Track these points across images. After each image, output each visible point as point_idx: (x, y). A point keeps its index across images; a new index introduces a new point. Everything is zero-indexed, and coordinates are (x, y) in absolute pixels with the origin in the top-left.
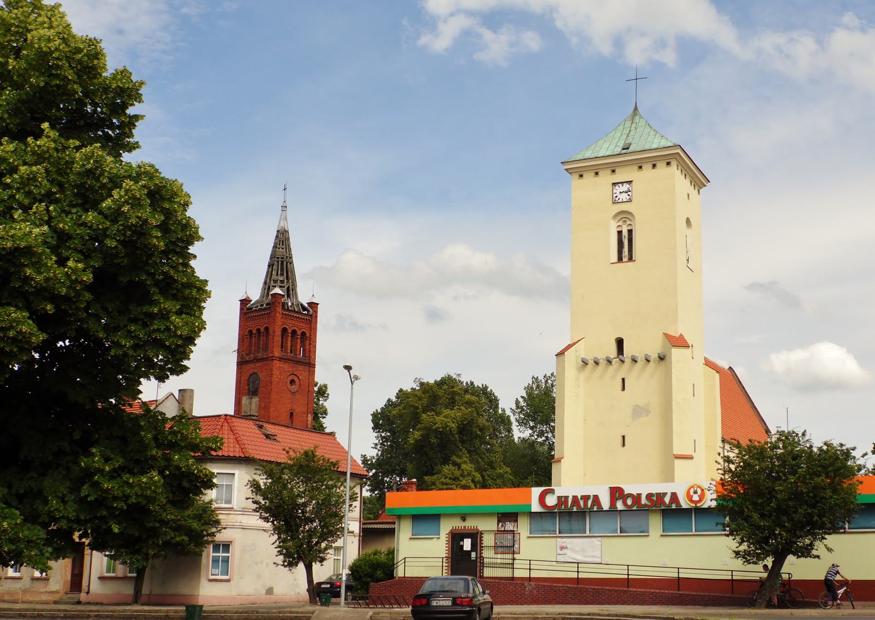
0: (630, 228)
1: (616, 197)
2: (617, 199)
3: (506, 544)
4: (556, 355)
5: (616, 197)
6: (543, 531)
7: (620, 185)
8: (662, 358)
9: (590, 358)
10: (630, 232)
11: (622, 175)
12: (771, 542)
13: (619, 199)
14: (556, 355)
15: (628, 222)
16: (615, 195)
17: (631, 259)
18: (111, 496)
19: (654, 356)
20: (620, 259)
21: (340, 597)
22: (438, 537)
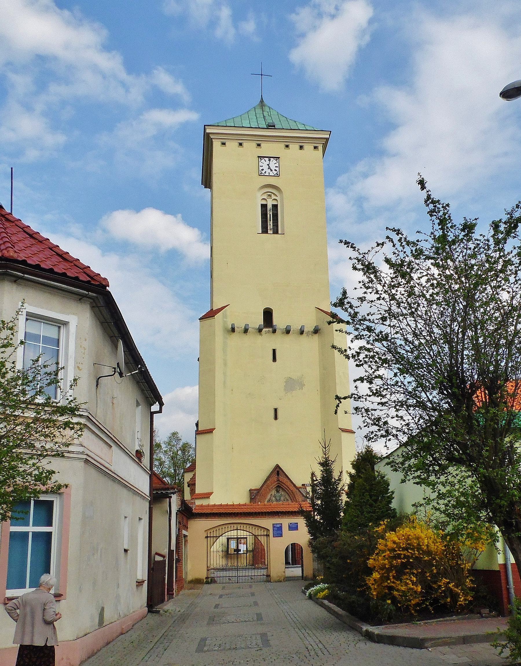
0: (275, 203)
1: (263, 170)
2: (263, 172)
3: (254, 528)
4: (199, 319)
5: (263, 170)
6: (138, 383)
7: (267, 159)
8: (316, 331)
9: (240, 325)
10: (275, 207)
11: (268, 149)
12: (444, 589)
13: (265, 172)
14: (199, 319)
15: (274, 197)
16: (261, 168)
17: (276, 232)
18: (403, 588)
19: (309, 327)
20: (265, 230)
21: (23, 648)
22: (11, 604)
